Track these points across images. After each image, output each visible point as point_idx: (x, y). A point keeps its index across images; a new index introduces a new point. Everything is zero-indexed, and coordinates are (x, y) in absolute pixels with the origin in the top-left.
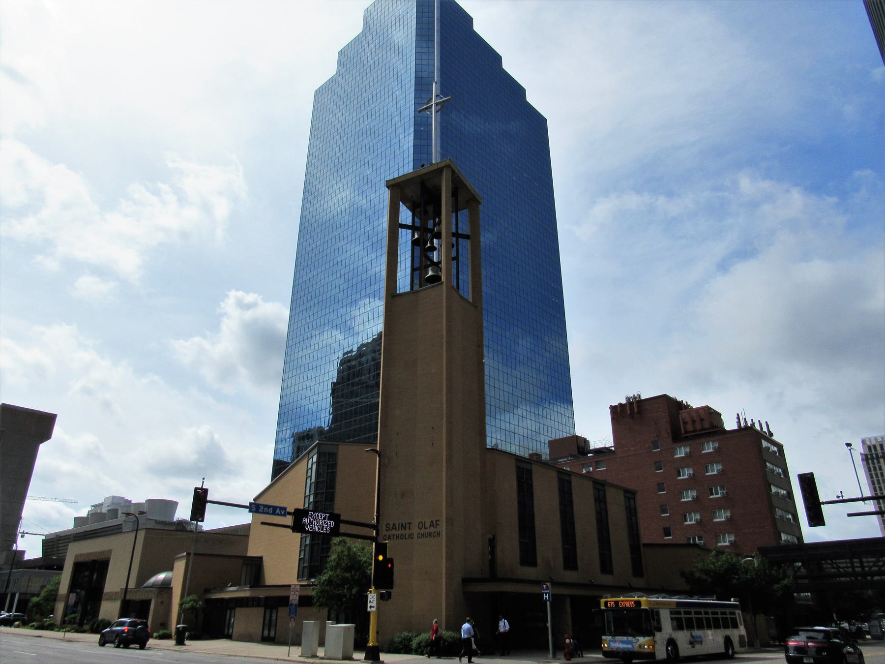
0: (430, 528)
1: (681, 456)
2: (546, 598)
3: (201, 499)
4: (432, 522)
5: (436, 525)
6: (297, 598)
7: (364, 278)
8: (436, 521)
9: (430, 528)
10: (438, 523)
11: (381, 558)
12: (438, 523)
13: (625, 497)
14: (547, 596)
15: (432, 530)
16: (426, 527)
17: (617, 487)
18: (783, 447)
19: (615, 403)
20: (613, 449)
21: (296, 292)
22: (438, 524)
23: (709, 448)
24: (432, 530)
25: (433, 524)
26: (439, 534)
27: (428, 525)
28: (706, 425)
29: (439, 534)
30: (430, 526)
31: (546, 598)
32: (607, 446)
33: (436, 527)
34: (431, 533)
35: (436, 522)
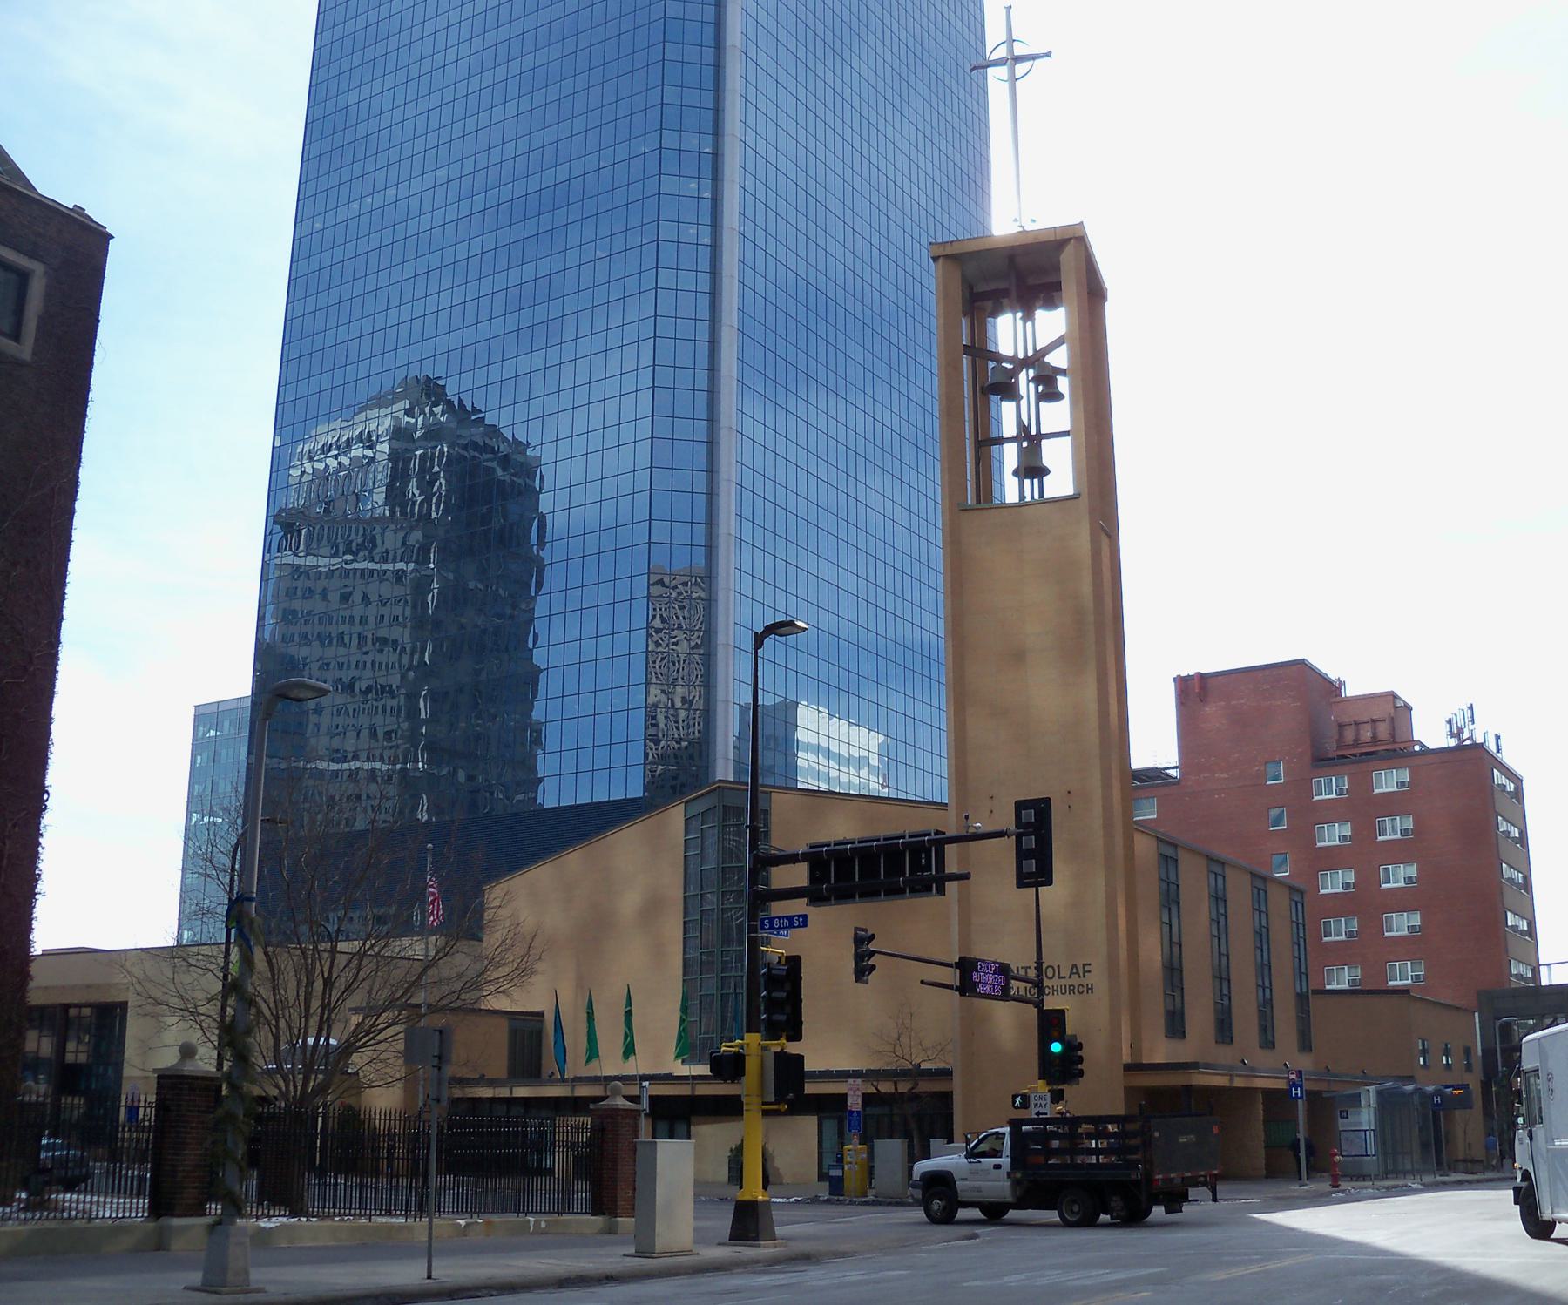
0: (1070, 977)
1: (1330, 797)
2: (1296, 1094)
3: (45, 826)
4: (1074, 966)
5: (1084, 972)
6: (860, 1101)
7: (412, 230)
8: (1084, 965)
9: (1070, 977)
10: (1087, 968)
11: (1056, 1047)
12: (1087, 968)
13: (1253, 886)
14: (1299, 1092)
15: (1075, 981)
16: (1062, 975)
17: (1240, 868)
18: (1522, 781)
19: (1175, 676)
20: (1173, 773)
21: (299, 294)
22: (1089, 972)
23: (1389, 781)
24: (1075, 981)
25: (1077, 970)
26: (1090, 989)
27: (1065, 972)
28: (1383, 730)
29: (1092, 989)
30: (1071, 973)
31: (1296, 1094)
32: (1159, 766)
33: (1084, 976)
34: (1074, 987)
35: (1084, 968)
